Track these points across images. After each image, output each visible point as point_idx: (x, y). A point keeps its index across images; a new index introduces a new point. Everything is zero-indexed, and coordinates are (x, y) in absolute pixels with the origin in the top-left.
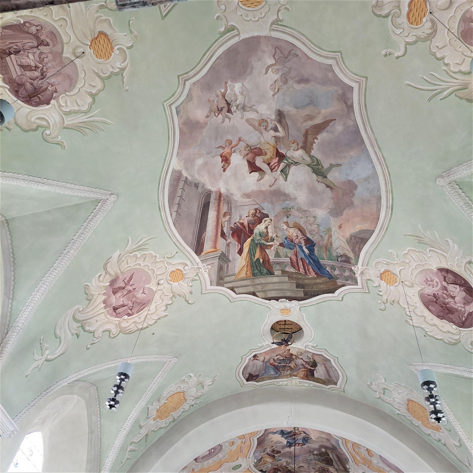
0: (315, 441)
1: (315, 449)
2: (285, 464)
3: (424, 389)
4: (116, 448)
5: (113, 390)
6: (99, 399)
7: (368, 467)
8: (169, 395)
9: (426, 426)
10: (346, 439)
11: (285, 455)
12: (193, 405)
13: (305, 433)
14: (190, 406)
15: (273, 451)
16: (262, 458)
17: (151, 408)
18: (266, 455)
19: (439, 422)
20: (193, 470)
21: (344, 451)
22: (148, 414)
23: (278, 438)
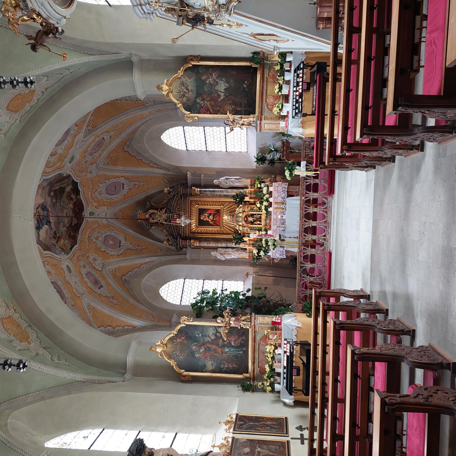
0: (45, 200)
1: (52, 201)
2: (65, 229)
3: (4, 87)
4: (57, 372)
5: (8, 370)
6: (10, 399)
7: (65, 158)
8: (6, 333)
9: (31, 100)
10: (43, 173)
11: (58, 228)
12: (15, 310)
13: (38, 208)
14: (16, 313)
15: (54, 237)
16: (60, 248)
17: (18, 348)
18: (58, 244)
19: (34, 82)
20: (73, 306)
21: (52, 176)
22: (25, 350)
23: (43, 232)
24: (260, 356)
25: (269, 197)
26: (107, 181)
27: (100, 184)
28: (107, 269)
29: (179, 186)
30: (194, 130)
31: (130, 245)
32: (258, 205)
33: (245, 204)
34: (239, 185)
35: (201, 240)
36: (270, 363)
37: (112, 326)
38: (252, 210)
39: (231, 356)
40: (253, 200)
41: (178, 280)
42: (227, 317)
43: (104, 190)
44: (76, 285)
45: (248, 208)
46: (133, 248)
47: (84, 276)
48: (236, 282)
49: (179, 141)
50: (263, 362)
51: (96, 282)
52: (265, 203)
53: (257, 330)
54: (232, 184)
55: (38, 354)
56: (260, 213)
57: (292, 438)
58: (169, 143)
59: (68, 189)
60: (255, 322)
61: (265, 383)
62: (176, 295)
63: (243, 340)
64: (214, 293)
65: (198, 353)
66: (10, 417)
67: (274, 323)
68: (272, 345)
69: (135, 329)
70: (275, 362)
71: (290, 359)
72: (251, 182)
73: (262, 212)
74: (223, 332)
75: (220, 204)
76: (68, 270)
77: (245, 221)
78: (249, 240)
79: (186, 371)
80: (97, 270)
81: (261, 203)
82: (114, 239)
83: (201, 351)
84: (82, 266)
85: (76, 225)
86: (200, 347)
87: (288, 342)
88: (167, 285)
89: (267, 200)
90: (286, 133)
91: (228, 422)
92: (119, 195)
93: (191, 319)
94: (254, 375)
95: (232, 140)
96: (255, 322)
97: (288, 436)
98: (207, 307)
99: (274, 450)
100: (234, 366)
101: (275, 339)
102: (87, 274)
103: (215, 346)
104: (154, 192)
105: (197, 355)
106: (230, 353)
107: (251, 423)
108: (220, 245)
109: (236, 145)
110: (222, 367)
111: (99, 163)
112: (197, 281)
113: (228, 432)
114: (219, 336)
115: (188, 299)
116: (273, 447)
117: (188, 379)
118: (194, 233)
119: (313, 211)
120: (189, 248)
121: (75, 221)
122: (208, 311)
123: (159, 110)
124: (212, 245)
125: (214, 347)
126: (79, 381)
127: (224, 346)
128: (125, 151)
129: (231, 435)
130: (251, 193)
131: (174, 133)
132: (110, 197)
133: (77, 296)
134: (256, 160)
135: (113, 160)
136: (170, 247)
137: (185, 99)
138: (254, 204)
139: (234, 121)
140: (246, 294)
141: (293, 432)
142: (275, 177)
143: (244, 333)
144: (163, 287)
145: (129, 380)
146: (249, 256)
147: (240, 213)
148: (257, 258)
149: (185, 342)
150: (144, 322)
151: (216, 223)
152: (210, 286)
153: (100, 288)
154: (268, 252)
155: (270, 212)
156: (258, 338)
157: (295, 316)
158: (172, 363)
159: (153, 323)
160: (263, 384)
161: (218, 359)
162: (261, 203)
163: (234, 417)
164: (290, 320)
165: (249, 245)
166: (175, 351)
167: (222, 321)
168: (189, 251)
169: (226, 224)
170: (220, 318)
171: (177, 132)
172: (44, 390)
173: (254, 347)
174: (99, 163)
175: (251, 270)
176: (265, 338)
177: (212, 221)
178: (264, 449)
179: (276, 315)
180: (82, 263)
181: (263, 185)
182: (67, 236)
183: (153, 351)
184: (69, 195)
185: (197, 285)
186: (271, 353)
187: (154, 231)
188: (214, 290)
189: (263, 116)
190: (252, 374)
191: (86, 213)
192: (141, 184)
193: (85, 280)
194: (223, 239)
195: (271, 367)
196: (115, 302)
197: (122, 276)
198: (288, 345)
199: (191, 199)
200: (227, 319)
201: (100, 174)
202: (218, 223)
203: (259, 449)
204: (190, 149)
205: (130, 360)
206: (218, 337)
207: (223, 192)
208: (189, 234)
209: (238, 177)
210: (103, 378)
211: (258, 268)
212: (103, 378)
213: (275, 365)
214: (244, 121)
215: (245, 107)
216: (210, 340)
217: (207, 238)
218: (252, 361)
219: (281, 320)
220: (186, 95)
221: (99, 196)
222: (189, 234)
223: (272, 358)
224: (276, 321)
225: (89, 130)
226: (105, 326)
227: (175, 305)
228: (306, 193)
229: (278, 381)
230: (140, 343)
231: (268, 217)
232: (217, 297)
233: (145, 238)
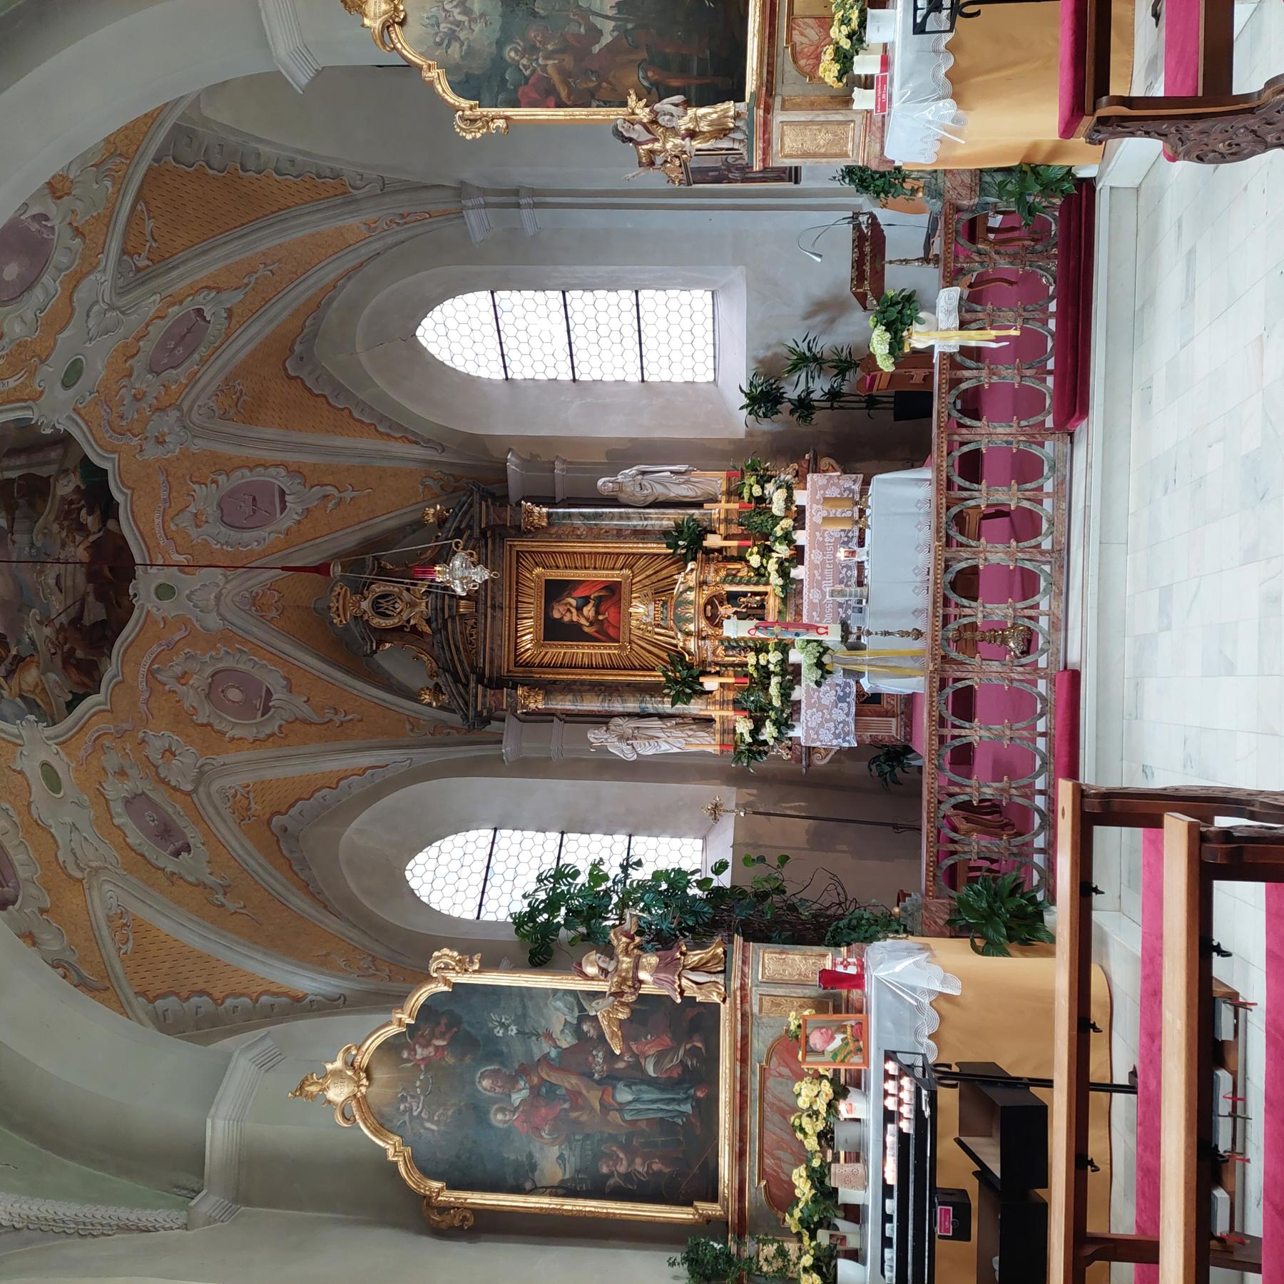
7: (43, 362)
16: (21, 696)
20: (43, 911)
24: (768, 1125)
25: (795, 528)
26: (222, 479)
27: (196, 487)
28: (215, 786)
29: (476, 497)
30: (530, 305)
31: (306, 708)
32: (755, 560)
33: (708, 561)
34: (685, 493)
35: (549, 688)
36: (816, 1163)
37: (210, 995)
38: (732, 578)
39: (643, 1125)
40: (734, 543)
41: (472, 834)
42: (627, 953)
43: (211, 511)
44: (75, 836)
45: (717, 571)
46: (317, 720)
47: (118, 808)
48: (676, 841)
49: (479, 348)
50: (780, 1154)
51: (165, 832)
52: (782, 551)
53: (756, 1009)
54: (660, 492)
56: (761, 589)
58: (443, 356)
59: (66, 487)
60: (744, 975)
61: (791, 1247)
62: (462, 885)
63: (693, 1052)
64: (597, 875)
65: (502, 1110)
67: (829, 978)
68: (822, 1077)
69: (299, 1006)
70: (836, 1159)
71: (916, 1152)
72: (729, 480)
73: (767, 583)
74: (609, 1017)
75: (619, 565)
76: (46, 778)
77: (707, 618)
78: (722, 685)
79: (452, 1186)
80: (175, 789)
81: (766, 552)
82: (245, 682)
83: (517, 1098)
84: (110, 771)
85: (103, 624)
86: (512, 1081)
87: (906, 1070)
88: (432, 850)
89: (787, 538)
90: (874, 165)
92: (268, 529)
93: (472, 962)
94: (741, 1210)
95: (663, 337)
96: (744, 975)
98: (560, 925)
100: (656, 1167)
101: (835, 1054)
102: (128, 802)
103: (574, 1081)
104: (391, 524)
105: (498, 1119)
106: (639, 1111)
108: (618, 706)
109: (676, 356)
110: (605, 1170)
111: (191, 409)
112: (540, 835)
114: (592, 1033)
115: (505, 900)
117: (457, 1223)
118: (527, 664)
119: (993, 500)
120: (511, 722)
121: (95, 612)
122: (572, 942)
123: (402, 216)
124: (592, 705)
125: (572, 1082)
127: (611, 1079)
128: (290, 378)
130: (728, 521)
131: (462, 317)
132: (235, 535)
133: (70, 876)
134: (745, 401)
135: (242, 403)
136: (444, 715)
137: (455, 51)
138: (741, 558)
139: (654, 122)
140: (711, 880)
142: (816, 459)
143: (696, 1021)
144: (420, 857)
145: (210, 1221)
146: (722, 744)
147: (690, 589)
148: (749, 751)
149: (450, 1060)
150: (333, 981)
151: (605, 632)
152: (583, 853)
153: (177, 854)
154: (792, 727)
155: (794, 581)
156: (759, 1046)
157: (925, 948)
158: (391, 1147)
159: (371, 985)
160: (782, 1253)
161: (587, 1136)
162: (766, 552)
164: (908, 962)
165: (723, 704)
166: (404, 1099)
167: (605, 972)
168: (511, 729)
169: (639, 633)
170: (593, 956)
171: (472, 311)
174: (191, 409)
175: (729, 795)
176: (793, 1043)
177: (592, 624)
179: (838, 945)
180: (112, 761)
181: (770, 487)
182: (58, 660)
183: (312, 1096)
184: (69, 512)
185: (538, 851)
186: (817, 1113)
187: (391, 659)
188: (595, 866)
189: (778, 100)
190: (733, 1205)
191: (143, 587)
192: (349, 495)
193: (116, 821)
194: (629, 684)
195: (818, 1177)
196: (232, 906)
197: (273, 815)
198: (905, 1081)
199: (520, 545)
200: (626, 962)
201: (194, 449)
202: (611, 632)
204: (517, 376)
205: (219, 1134)
206: (587, 1039)
207: (629, 518)
208: (512, 667)
209: (682, 468)
210: (101, 1212)
211: (754, 791)
212: (101, 1212)
213: (839, 1174)
214: (696, 119)
215: (702, 74)
216: (553, 1053)
217: (574, 682)
218: (732, 1146)
219: (861, 966)
220: (462, 35)
221: (193, 532)
222: (512, 667)
223: (821, 1136)
224: (840, 969)
225: (138, 270)
226: (184, 994)
227: (460, 921)
228: (961, 425)
229: (853, 1242)
230: (268, 1064)
231: (791, 603)
232: (607, 892)
233: (359, 685)
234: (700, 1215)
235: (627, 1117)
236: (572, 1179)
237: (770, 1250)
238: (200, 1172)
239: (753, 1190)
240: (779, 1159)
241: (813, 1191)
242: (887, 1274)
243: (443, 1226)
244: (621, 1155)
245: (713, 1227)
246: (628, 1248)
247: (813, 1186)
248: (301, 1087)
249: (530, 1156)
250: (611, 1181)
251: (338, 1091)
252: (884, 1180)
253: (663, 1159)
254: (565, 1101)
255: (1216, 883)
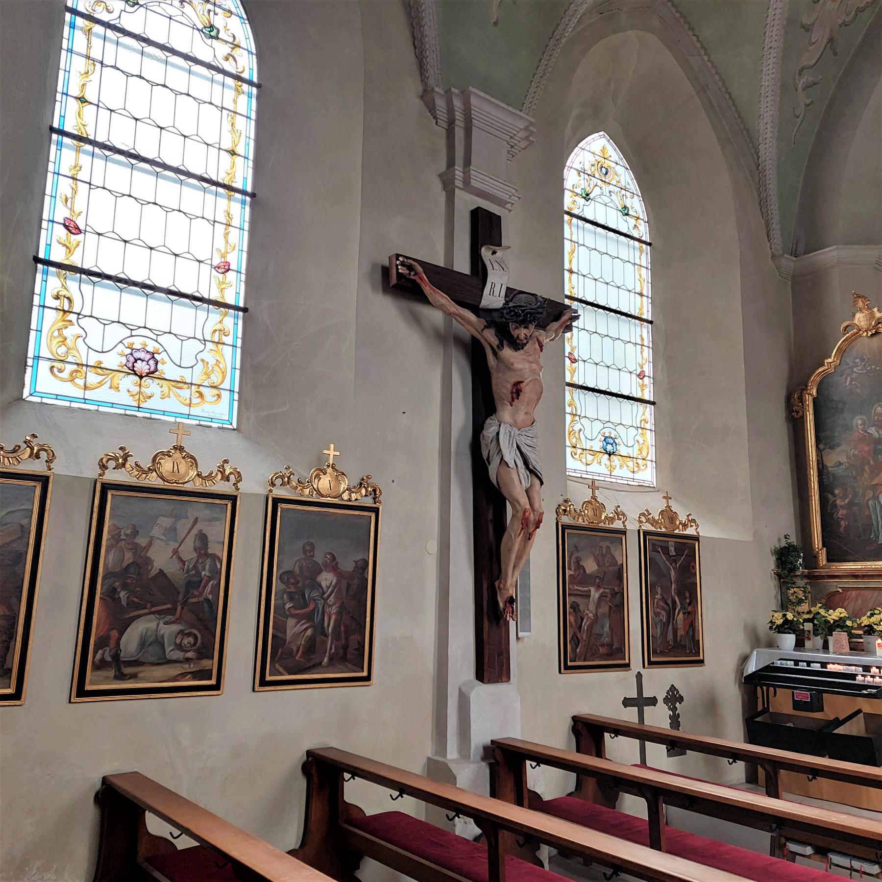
39: (867, 513)
50: (860, 602)
55: (807, 30)
57: (639, 676)
65: (864, 423)
66: (641, 33)
71: (846, 685)
79: (815, 400)
83: (872, 430)
91: (669, 515)
94: (823, 577)
97: (644, 667)
99: (597, 630)
100: (842, 523)
105: (858, 421)
107: (673, 573)
110: (836, 492)
113: (643, 519)
116: (607, 628)
117: (795, 408)
126: (757, 154)
129: (632, 526)
141: (660, 679)
161: (855, 478)
163: (690, 531)
166: (862, 360)
172: (724, 83)
173: (872, 577)
178: (597, 608)
183: (855, 304)
190: (823, 572)
195: (839, 624)
203: (595, 594)
205: (829, 255)
229: (808, 644)
234: (818, 552)
235: (870, 503)
236: (829, 472)
237: (801, 595)
238: (807, 252)
239: (835, 584)
240: (856, 600)
241: (832, 622)
242: (779, 662)
243: (792, 400)
244: (847, 501)
245: (811, 560)
246: (794, 510)
247: (835, 621)
248: (859, 297)
249: (839, 445)
250: (830, 496)
251: (862, 319)
252: (829, 663)
253: (847, 527)
254: (874, 461)
255: (636, 708)
